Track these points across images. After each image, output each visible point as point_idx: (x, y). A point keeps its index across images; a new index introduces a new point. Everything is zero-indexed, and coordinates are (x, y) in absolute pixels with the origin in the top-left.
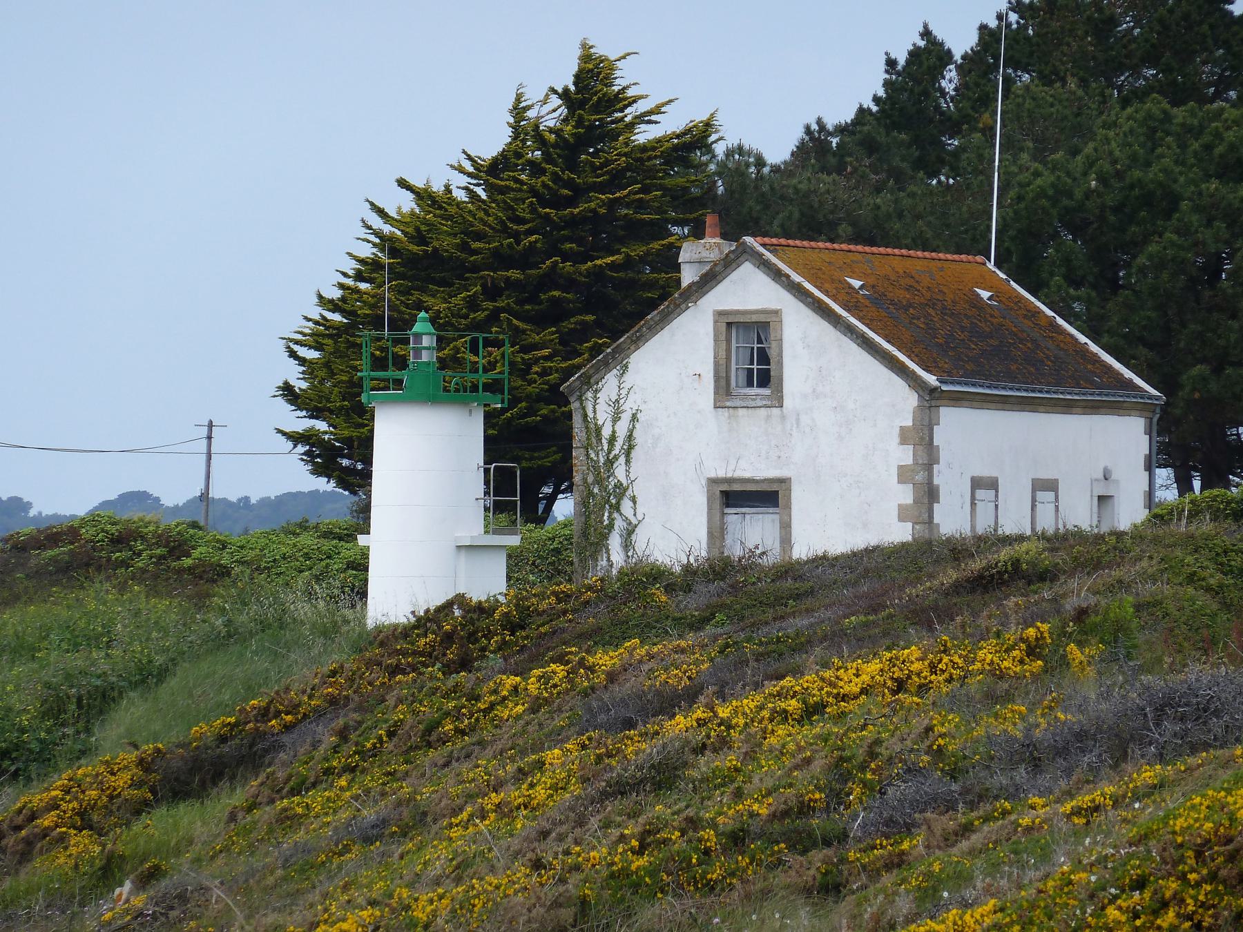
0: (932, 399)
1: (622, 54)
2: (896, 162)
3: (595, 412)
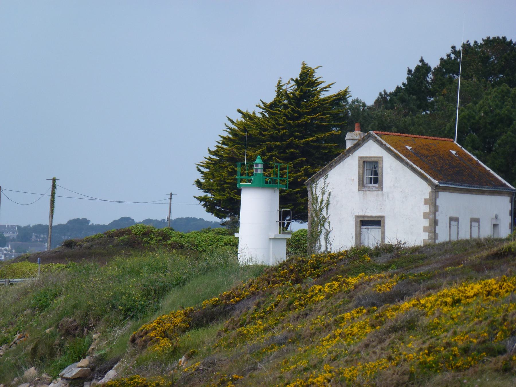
0: (436, 189)
1: (316, 67)
2: (411, 105)
3: (316, 192)
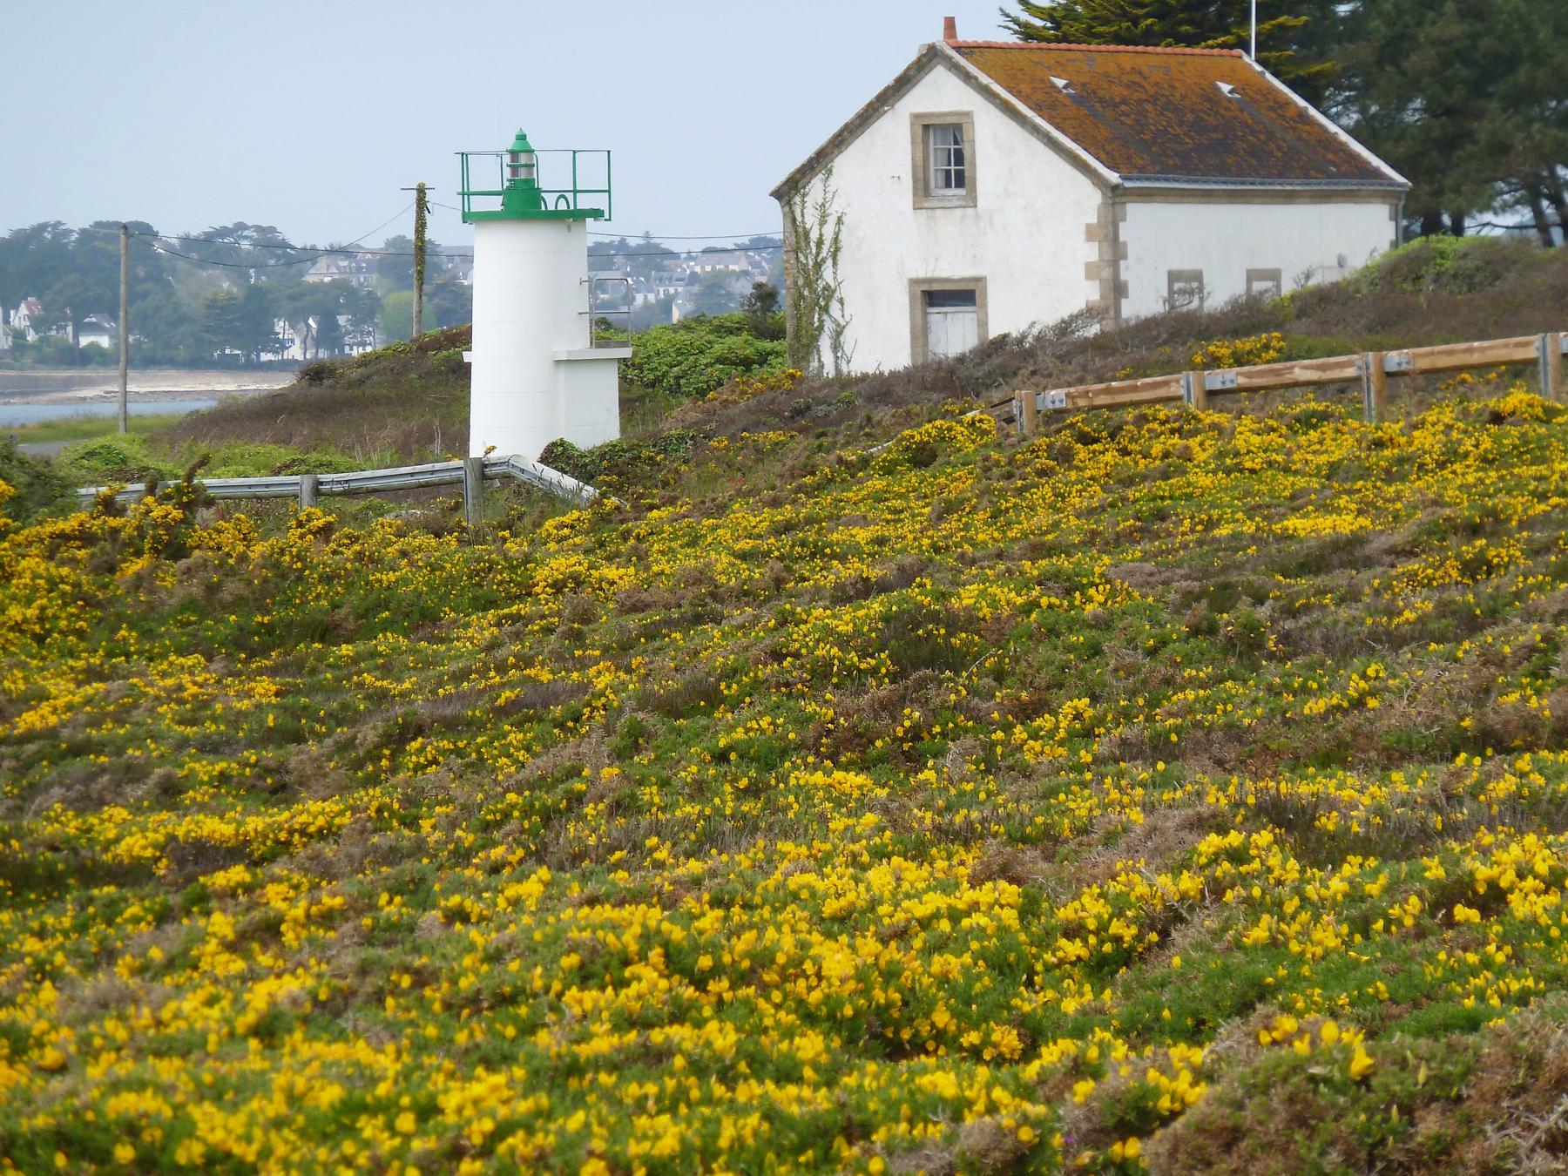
0: (1116, 196)
